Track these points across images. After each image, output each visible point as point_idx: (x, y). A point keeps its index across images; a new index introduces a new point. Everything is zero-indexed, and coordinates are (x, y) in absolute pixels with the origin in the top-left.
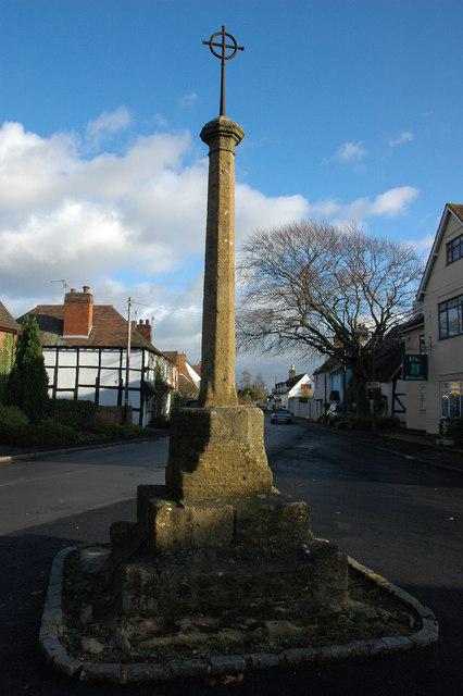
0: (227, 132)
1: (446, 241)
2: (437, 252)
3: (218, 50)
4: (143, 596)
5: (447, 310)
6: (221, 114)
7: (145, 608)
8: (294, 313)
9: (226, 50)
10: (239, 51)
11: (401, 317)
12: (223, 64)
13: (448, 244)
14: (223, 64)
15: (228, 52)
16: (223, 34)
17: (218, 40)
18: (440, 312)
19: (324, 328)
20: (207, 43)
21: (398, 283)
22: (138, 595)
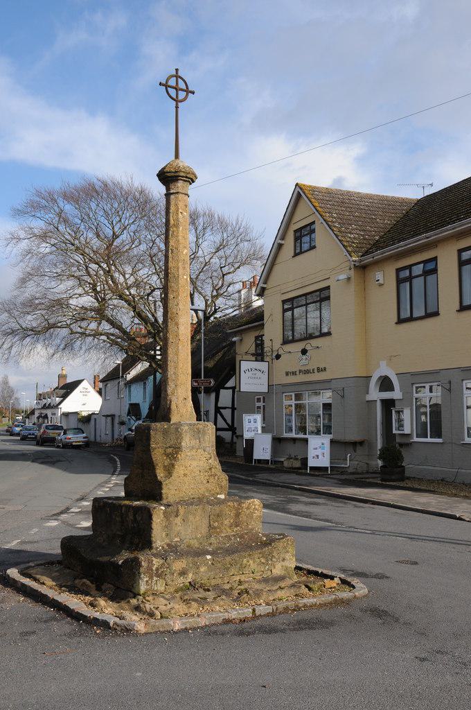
0: (186, 177)
1: (294, 227)
2: (283, 238)
3: (173, 92)
4: (155, 578)
5: (292, 309)
6: (177, 156)
7: (155, 589)
8: (88, 301)
9: (180, 92)
10: (190, 95)
11: (231, 310)
12: (177, 107)
13: (295, 231)
14: (177, 107)
15: (182, 95)
16: (177, 77)
17: (172, 82)
18: (285, 311)
19: (126, 318)
20: (163, 85)
21: (225, 270)
22: (151, 578)
